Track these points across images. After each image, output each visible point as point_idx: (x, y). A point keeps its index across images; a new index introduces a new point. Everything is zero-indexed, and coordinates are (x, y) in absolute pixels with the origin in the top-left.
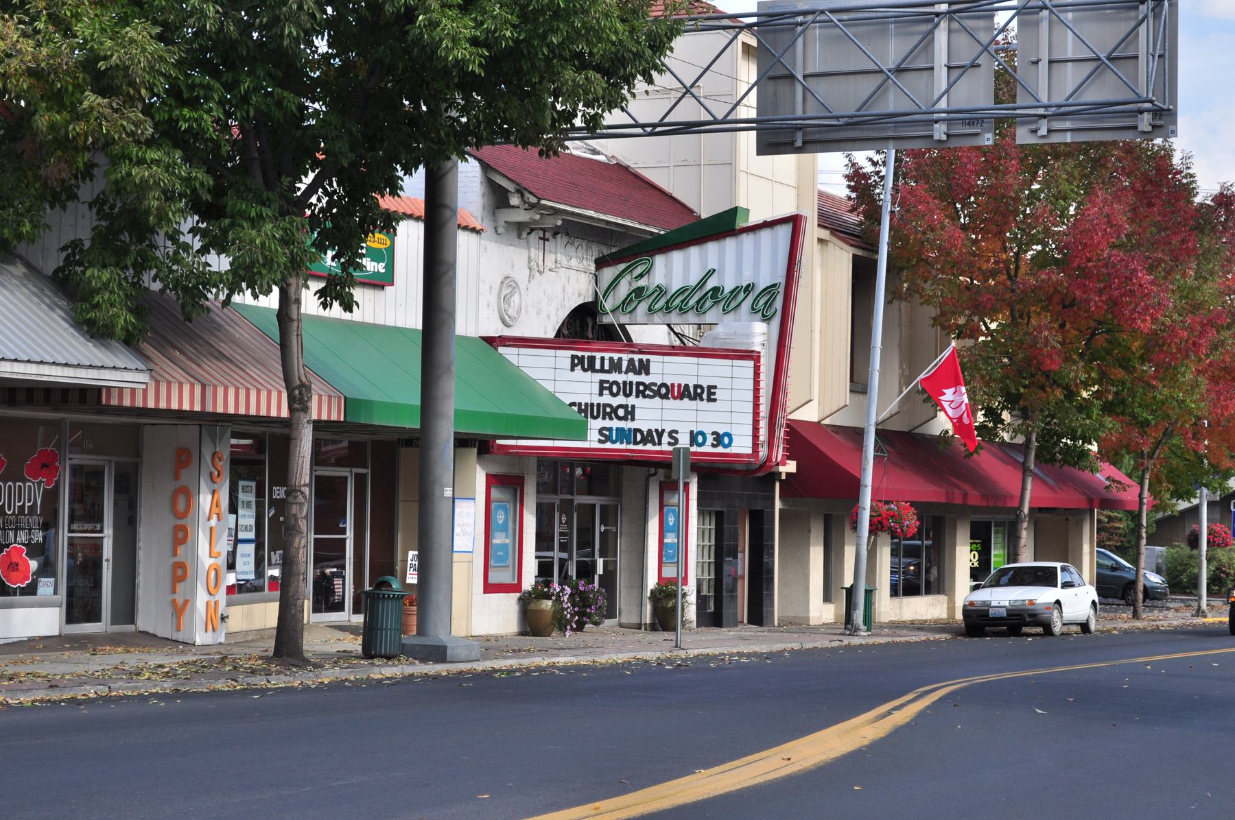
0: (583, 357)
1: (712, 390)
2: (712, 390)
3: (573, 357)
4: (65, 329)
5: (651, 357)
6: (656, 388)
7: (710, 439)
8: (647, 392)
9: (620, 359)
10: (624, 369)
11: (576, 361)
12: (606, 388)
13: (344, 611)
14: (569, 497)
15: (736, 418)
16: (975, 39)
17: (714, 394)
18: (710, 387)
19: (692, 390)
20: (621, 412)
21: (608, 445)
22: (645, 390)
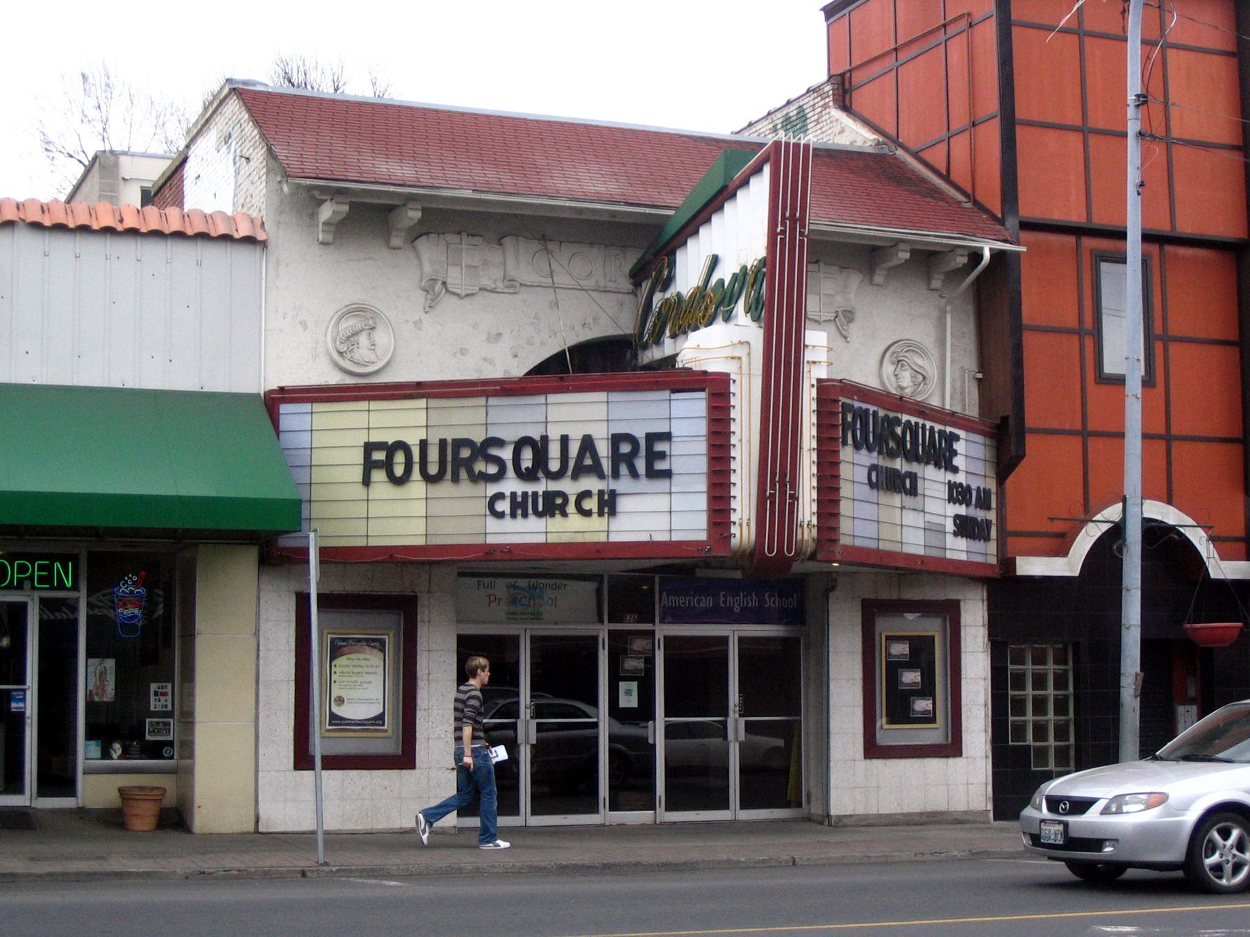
4: (920, 830)
8: (480, 466)
12: (378, 465)
16: (987, 120)
17: (662, 456)
18: (652, 438)
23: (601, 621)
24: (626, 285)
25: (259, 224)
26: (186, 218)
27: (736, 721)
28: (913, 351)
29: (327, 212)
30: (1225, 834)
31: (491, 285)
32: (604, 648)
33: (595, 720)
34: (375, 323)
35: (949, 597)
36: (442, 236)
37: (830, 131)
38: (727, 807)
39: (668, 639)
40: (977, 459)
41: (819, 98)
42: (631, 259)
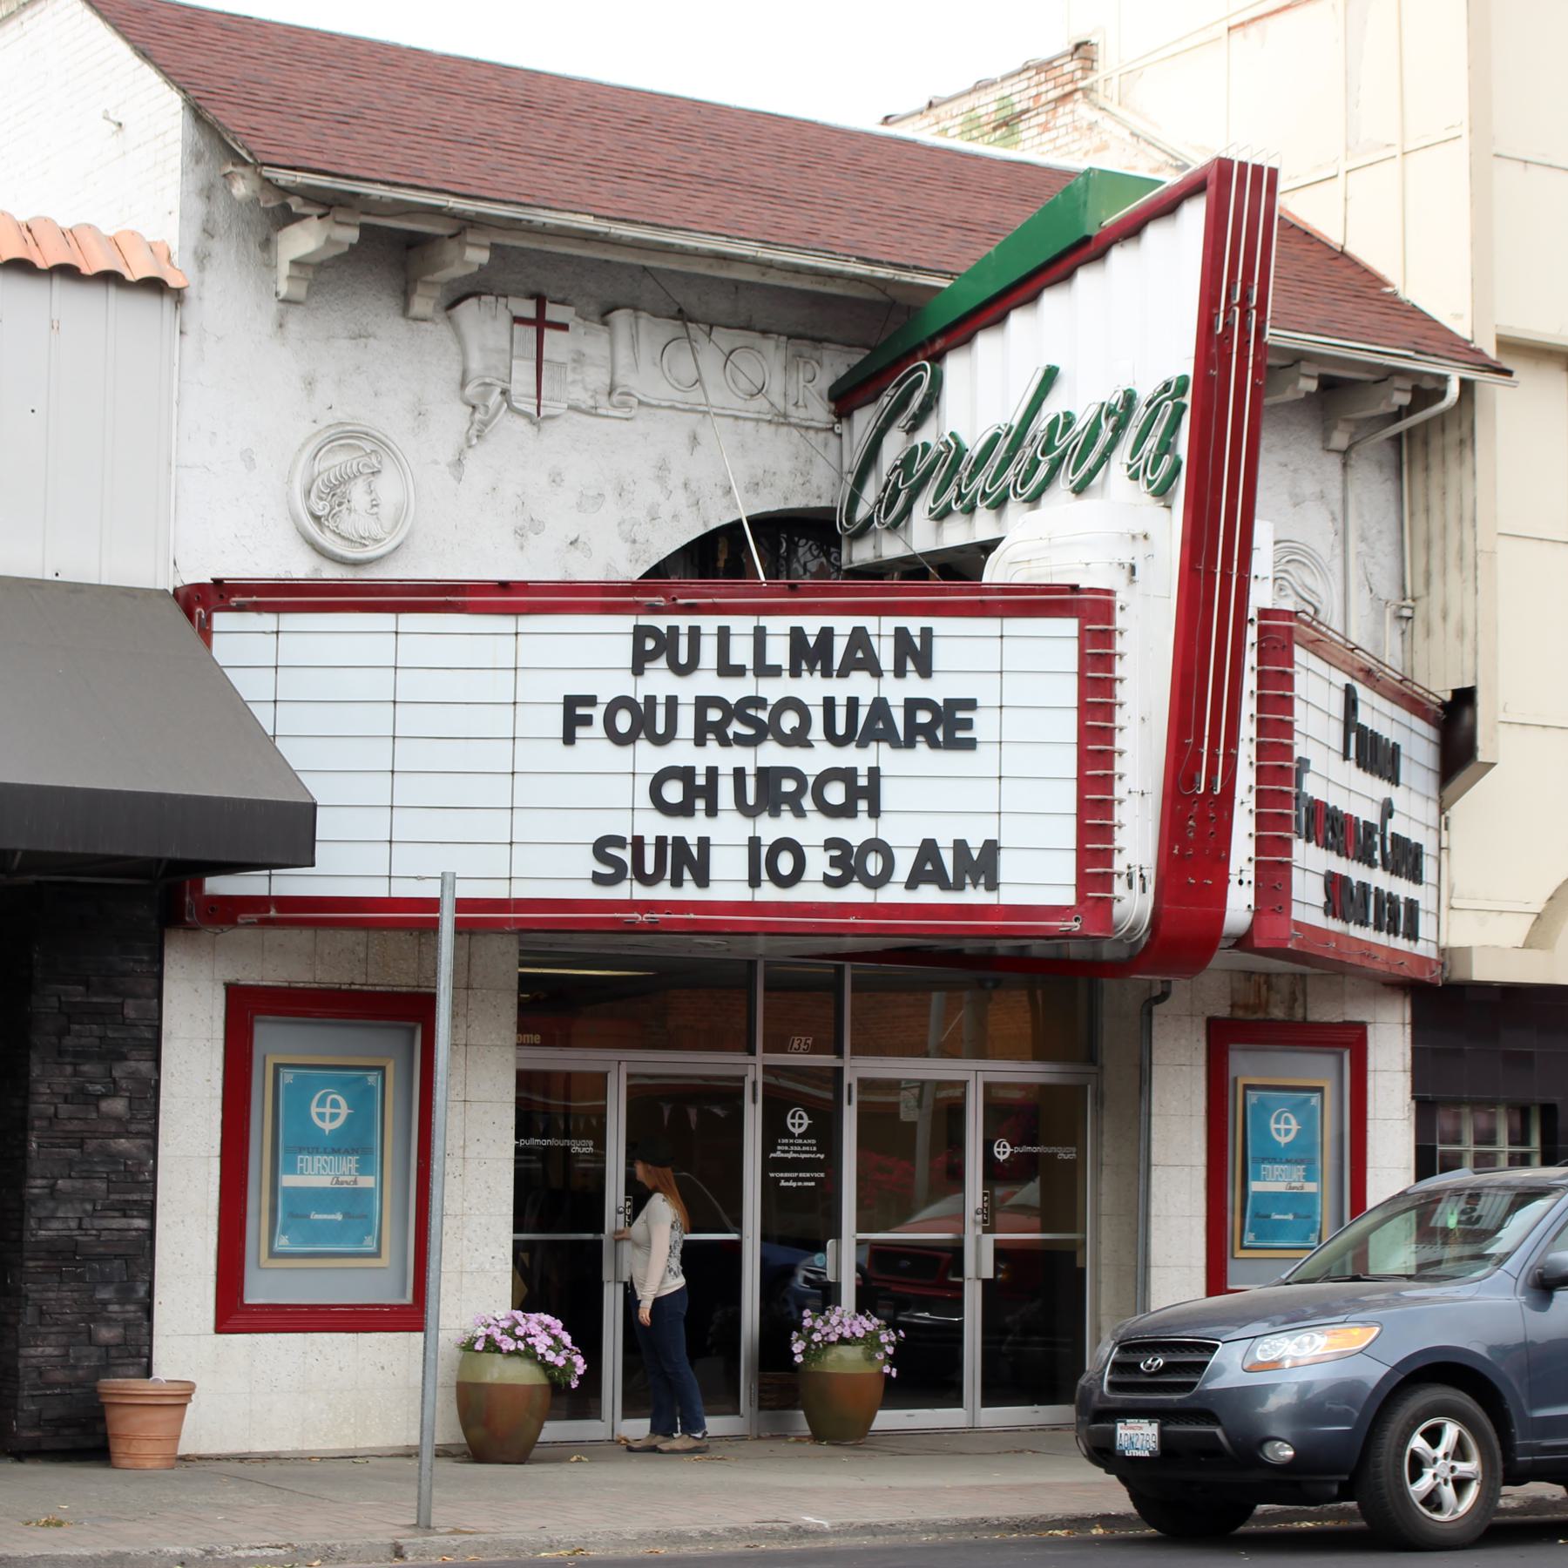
0: (674, 630)
1: (580, 711)
2: (580, 711)
3: (640, 633)
5: (939, 625)
6: (764, 715)
7: (818, 863)
9: (827, 635)
10: (836, 664)
11: (650, 644)
13: (598, 1416)
14: (826, 1060)
15: (1015, 797)
19: (898, 717)
20: (835, 794)
21: (628, 890)
22: (725, 722)
23: (752, 1053)
24: (820, 412)
25: (165, 257)
26: (69, 236)
27: (978, 1239)
28: (1300, 562)
29: (303, 240)
30: (1433, 1437)
31: (586, 401)
32: (754, 1101)
33: (734, 1236)
34: (380, 463)
35: (1348, 1018)
36: (503, 300)
37: (1073, 147)
38: (958, 1402)
39: (866, 1085)
40: (1423, 765)
41: (1051, 84)
42: (834, 366)
